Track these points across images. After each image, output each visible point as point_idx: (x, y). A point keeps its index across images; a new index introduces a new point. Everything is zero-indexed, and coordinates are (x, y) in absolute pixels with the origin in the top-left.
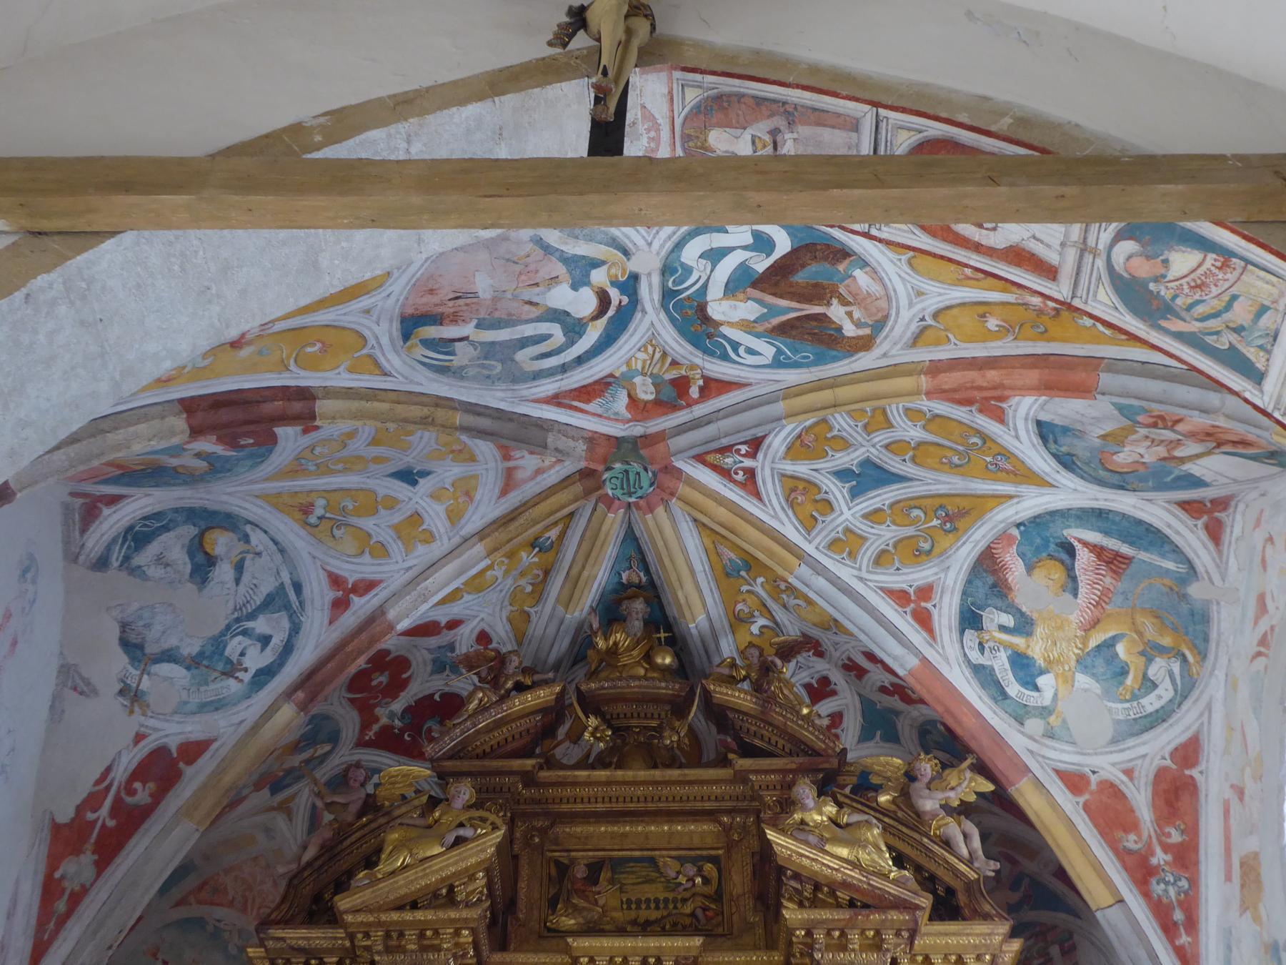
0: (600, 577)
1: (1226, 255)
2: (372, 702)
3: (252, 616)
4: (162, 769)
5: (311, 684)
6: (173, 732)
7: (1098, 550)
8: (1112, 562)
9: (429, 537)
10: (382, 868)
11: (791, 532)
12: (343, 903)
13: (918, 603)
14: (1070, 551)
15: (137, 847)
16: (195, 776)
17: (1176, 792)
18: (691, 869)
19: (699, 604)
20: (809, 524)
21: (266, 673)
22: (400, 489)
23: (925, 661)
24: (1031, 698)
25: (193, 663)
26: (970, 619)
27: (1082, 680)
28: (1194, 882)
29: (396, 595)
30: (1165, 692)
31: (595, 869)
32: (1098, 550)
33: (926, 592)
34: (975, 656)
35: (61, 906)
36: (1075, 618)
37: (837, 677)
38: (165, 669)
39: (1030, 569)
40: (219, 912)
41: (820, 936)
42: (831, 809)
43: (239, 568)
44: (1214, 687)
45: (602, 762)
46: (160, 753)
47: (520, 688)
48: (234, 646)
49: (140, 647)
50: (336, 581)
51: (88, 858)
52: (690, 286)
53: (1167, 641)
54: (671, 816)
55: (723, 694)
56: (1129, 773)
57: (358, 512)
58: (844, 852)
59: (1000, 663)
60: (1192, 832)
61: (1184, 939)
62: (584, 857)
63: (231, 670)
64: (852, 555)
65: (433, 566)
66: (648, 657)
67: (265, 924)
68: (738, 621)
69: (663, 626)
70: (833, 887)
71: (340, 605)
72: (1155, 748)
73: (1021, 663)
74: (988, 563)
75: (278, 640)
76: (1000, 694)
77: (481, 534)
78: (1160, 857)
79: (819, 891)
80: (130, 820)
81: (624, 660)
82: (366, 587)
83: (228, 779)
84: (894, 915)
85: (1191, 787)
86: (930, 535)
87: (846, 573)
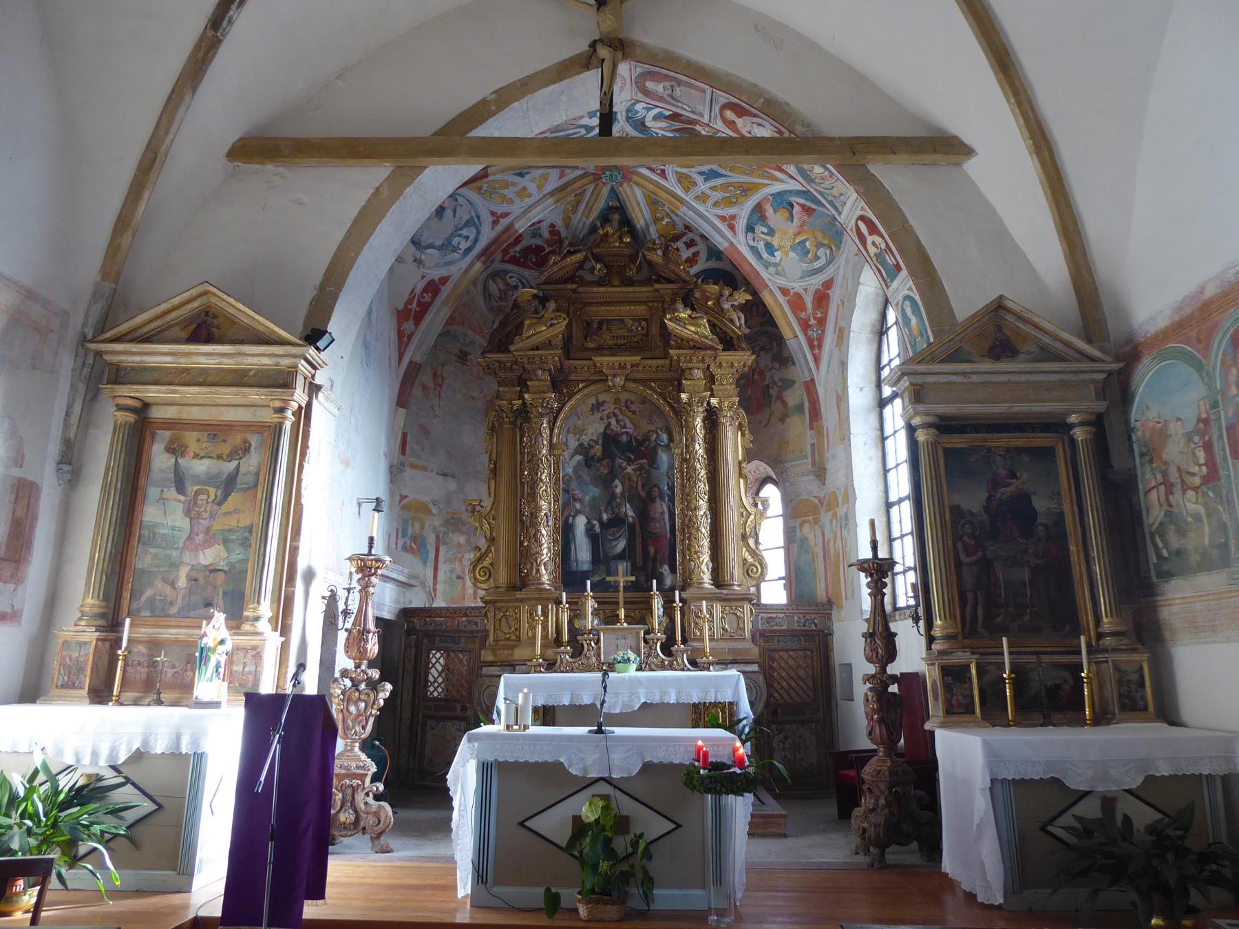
0: (601, 204)
1: (832, 174)
2: (561, 440)
3: (461, 229)
4: (433, 288)
5: (486, 253)
6: (436, 274)
7: (803, 206)
8: (808, 211)
9: (530, 195)
10: (525, 335)
11: (679, 192)
12: (512, 348)
13: (730, 222)
14: (792, 206)
15: (429, 317)
16: (446, 289)
17: (822, 298)
18: (637, 324)
19: (641, 215)
20: (687, 190)
21: (469, 250)
22: (518, 179)
23: (732, 244)
24: (772, 260)
25: (440, 248)
26: (750, 229)
27: (792, 254)
28: (823, 332)
29: (518, 218)
30: (823, 261)
31: (601, 323)
32: (803, 206)
33: (733, 217)
34: (751, 242)
35: (405, 340)
36: (791, 231)
37: (698, 239)
38: (429, 251)
39: (775, 211)
40: (454, 327)
41: (682, 359)
42: (689, 312)
43: (455, 211)
44: (841, 261)
45: (599, 283)
46: (432, 282)
47: (570, 253)
48: (455, 241)
49: (419, 243)
50: (493, 213)
51: (411, 323)
52: (639, 116)
53: (826, 242)
54: (629, 303)
55: (650, 256)
56: (805, 290)
57: (501, 188)
58: (693, 329)
59: (761, 246)
60: (825, 313)
61: (816, 351)
62: (596, 319)
63: (455, 250)
64: (704, 202)
65: (532, 206)
66: (620, 238)
67: (484, 353)
68: (657, 220)
69: (627, 222)
70: (688, 341)
71: (495, 223)
72: (817, 281)
73: (769, 246)
74: (759, 209)
75: (472, 237)
76: (759, 257)
77: (552, 194)
78: (812, 322)
79: (683, 343)
80: (424, 308)
81: (611, 239)
82: (505, 215)
83: (459, 291)
84: (709, 352)
85: (828, 296)
86: (736, 197)
87: (701, 208)
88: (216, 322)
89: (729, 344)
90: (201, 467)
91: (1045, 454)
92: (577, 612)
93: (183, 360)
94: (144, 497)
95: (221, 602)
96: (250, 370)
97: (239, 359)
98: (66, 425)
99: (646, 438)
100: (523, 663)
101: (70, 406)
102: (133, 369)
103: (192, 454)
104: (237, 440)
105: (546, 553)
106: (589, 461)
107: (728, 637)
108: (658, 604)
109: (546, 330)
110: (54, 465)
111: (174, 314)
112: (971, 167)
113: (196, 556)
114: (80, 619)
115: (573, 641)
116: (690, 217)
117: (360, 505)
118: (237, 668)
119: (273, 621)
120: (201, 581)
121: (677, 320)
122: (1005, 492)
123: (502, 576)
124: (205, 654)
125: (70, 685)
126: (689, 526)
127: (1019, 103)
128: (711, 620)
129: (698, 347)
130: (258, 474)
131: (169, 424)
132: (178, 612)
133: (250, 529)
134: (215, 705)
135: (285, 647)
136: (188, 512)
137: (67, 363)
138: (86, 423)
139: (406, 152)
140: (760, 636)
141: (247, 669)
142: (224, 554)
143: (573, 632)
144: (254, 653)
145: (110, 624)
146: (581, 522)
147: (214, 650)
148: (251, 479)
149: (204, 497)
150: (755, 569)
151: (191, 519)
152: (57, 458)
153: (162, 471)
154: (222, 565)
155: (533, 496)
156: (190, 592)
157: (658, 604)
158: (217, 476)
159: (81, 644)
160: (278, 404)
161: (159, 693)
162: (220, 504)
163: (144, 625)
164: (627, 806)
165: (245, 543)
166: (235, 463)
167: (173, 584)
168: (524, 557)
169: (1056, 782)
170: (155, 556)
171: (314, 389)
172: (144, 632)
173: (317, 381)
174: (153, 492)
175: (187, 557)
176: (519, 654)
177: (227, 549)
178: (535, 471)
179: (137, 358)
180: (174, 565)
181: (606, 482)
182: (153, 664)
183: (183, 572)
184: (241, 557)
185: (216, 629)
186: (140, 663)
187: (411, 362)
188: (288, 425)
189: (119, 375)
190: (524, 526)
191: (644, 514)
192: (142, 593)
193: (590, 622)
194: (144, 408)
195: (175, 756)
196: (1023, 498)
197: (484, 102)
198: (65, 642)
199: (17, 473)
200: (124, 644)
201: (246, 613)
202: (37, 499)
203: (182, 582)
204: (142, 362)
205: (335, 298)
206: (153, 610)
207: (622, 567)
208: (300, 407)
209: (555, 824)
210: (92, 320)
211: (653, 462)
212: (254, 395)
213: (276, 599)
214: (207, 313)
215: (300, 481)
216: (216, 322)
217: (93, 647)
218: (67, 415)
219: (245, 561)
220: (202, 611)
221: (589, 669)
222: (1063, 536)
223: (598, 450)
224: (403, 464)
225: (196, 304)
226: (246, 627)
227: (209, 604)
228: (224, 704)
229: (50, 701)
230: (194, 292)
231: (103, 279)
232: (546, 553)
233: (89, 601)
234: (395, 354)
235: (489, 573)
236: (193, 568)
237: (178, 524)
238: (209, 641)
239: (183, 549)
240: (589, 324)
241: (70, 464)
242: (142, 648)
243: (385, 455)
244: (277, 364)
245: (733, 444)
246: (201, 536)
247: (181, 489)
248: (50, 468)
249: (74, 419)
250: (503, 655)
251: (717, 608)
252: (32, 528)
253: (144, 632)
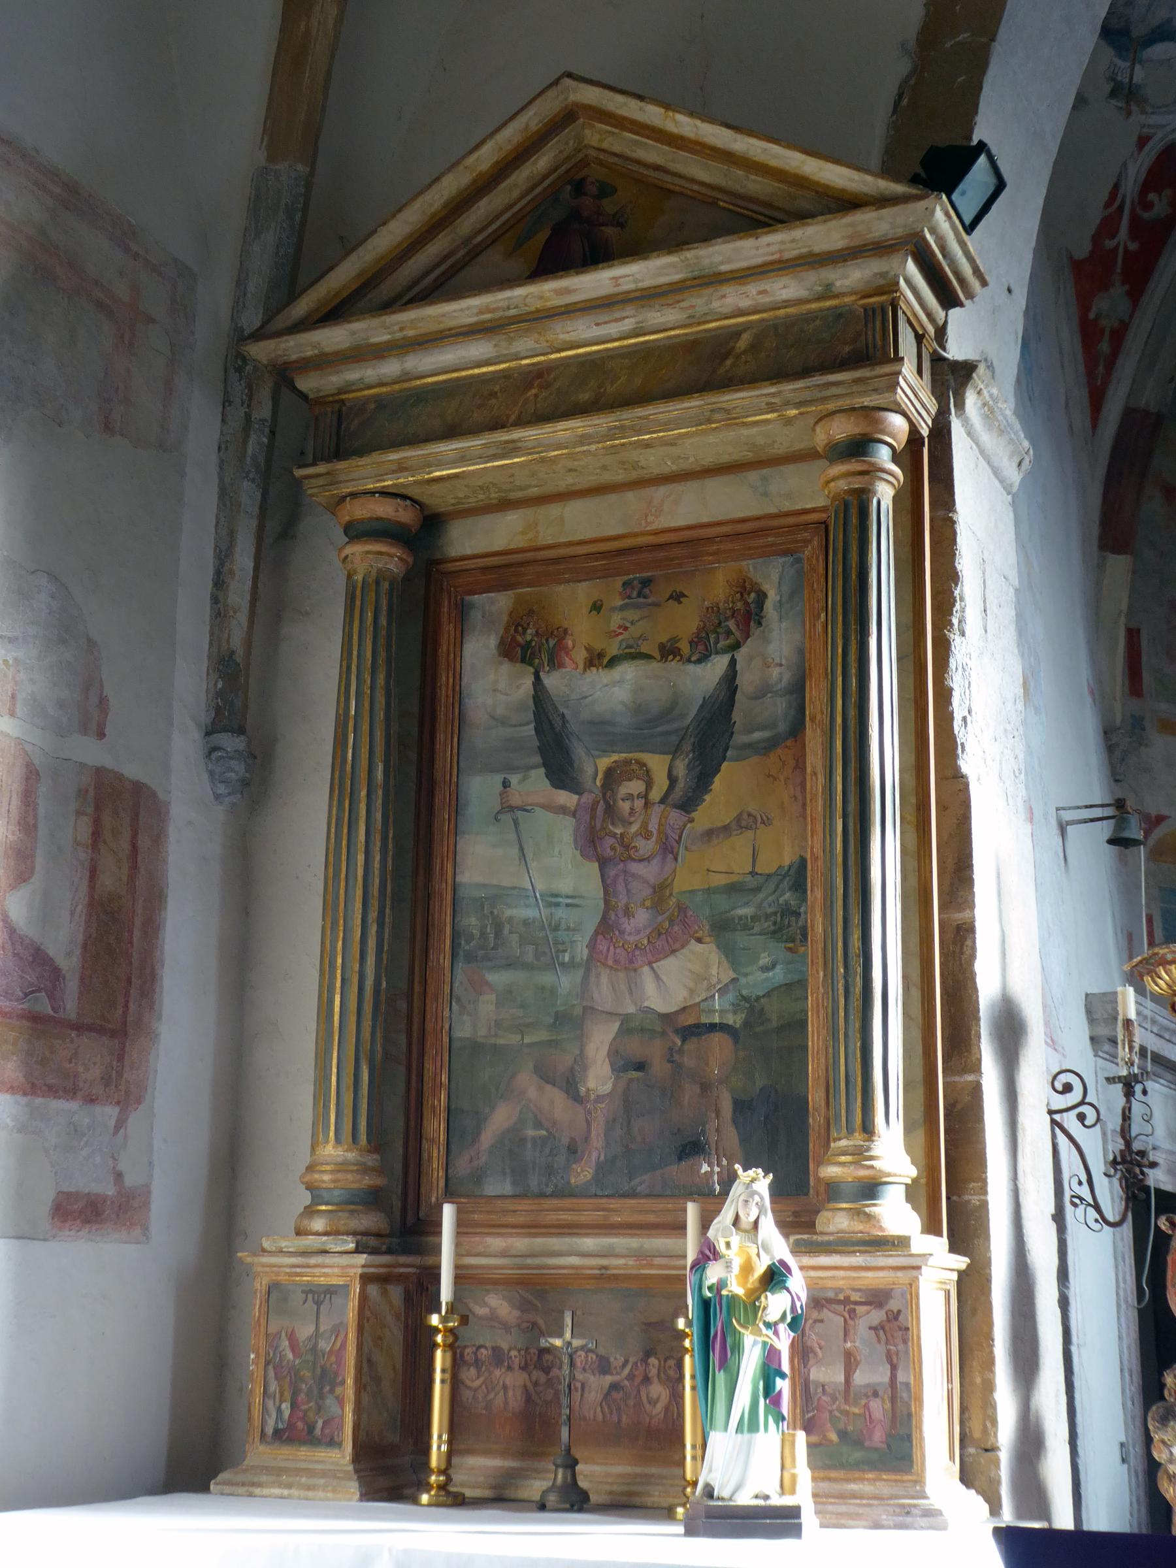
35: (1105, 347)
38: (1159, 50)
49: (1125, 32)
51: (1118, 291)
88: (609, 206)
90: (614, 691)
93: (524, 344)
94: (457, 808)
95: (731, 1137)
96: (737, 333)
97: (699, 302)
98: (220, 613)
101: (224, 555)
102: (381, 403)
103: (581, 655)
104: (716, 586)
110: (196, 735)
111: (484, 208)
113: (633, 988)
114: (310, 1212)
117: (1062, 828)
118: (827, 1374)
119: (923, 1194)
120: (659, 1068)
124: (718, 1324)
125: (297, 1433)
130: (798, 688)
131: (503, 571)
132: (598, 1179)
133: (797, 877)
134: (777, 1521)
135: (971, 1289)
136: (590, 842)
137: (201, 425)
138: (273, 606)
141: (860, 1378)
142: (719, 970)
144: (877, 1316)
145: (398, 1225)
147: (751, 1309)
148: (778, 708)
149: (635, 787)
151: (603, 863)
152: (206, 718)
153: (503, 722)
154: (720, 1009)
156: (628, 1106)
158: (667, 713)
159: (322, 1295)
160: (841, 429)
161: (571, 1464)
162: (688, 805)
163: (495, 1227)
165: (787, 928)
166: (719, 664)
167: (571, 1085)
170: (507, 996)
171: (950, 378)
172: (501, 1250)
173: (955, 351)
174: (479, 790)
175: (605, 990)
177: (729, 952)
179: (390, 368)
180: (570, 1022)
182: (540, 1360)
183: (600, 1041)
184: (778, 975)
185: (744, 1234)
186: (498, 1356)
187: (1129, 413)
188: (885, 494)
189: (345, 429)
192: (480, 1120)
194: (421, 530)
198: (273, 1288)
199: (92, 753)
200: (446, 1294)
201: (831, 1171)
202: (158, 839)
203: (599, 1078)
204: (406, 377)
205: (977, 63)
206: (519, 1173)
208: (914, 438)
210: (256, 284)
212: (762, 415)
213: (921, 1119)
214: (579, 187)
215: (944, 695)
216: (609, 206)
217: (353, 1304)
218: (220, 583)
219: (796, 987)
220: (676, 1171)
224: (1137, 725)
225: (542, 162)
226: (837, 1221)
227: (692, 1148)
228: (809, 1518)
229: (248, 1488)
230: (532, 119)
231: (272, 158)
233: (330, 1151)
234: (1081, 394)
236: (628, 1028)
237: (565, 886)
238: (730, 1274)
239: (588, 965)
241: (241, 731)
242: (497, 1304)
243: (1092, 693)
244: (828, 292)
246: (642, 917)
247: (561, 772)
248: (185, 745)
249: (239, 594)
252: (152, 928)
253: (501, 1250)
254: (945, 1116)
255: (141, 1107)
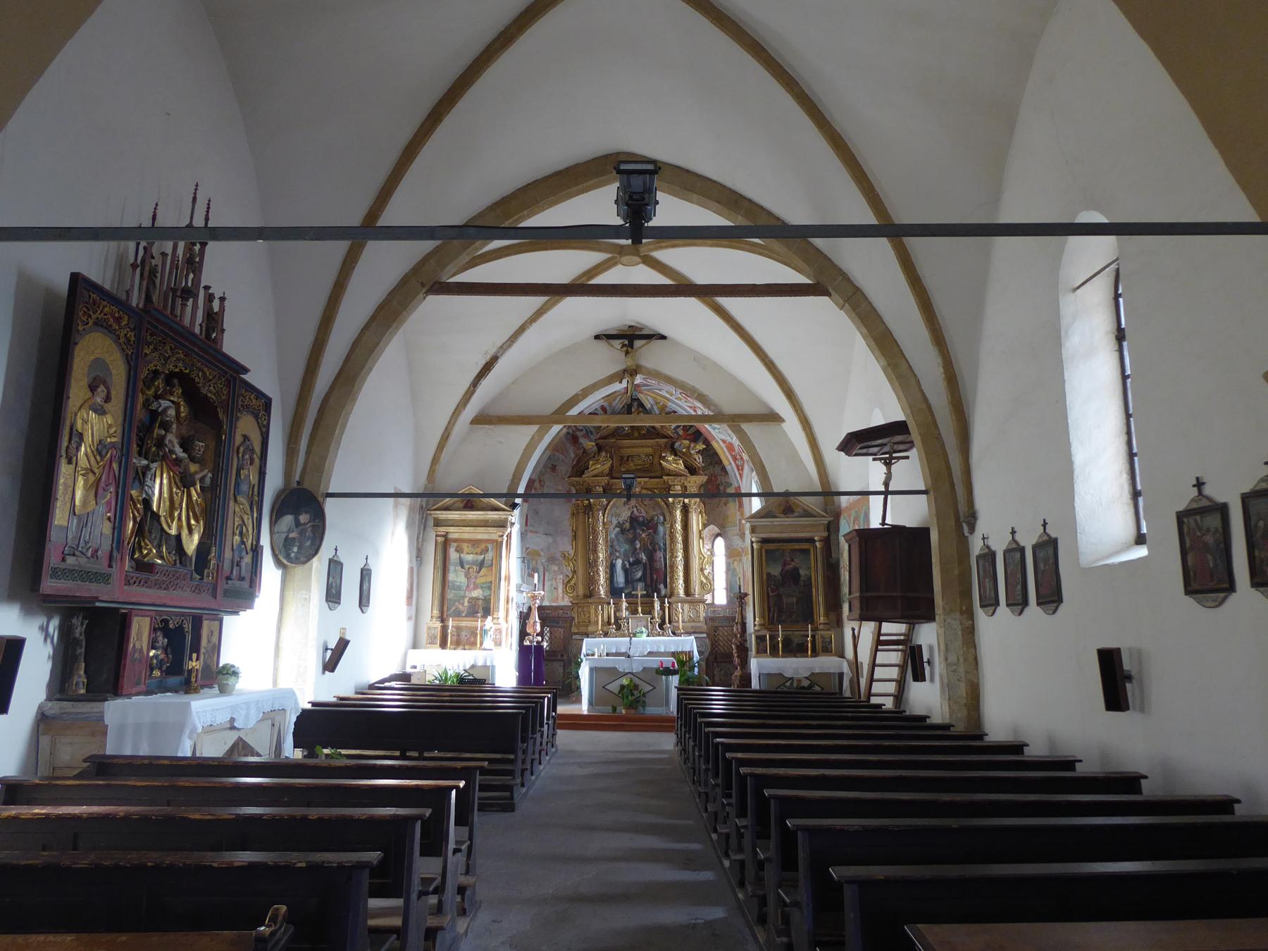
89: (692, 470)
90: (470, 558)
91: (806, 552)
92: (618, 609)
99: (652, 519)
100: (593, 633)
104: (483, 546)
105: (602, 580)
106: (623, 531)
107: (691, 620)
108: (657, 605)
109: (600, 466)
112: (784, 425)
115: (616, 622)
116: (674, 407)
121: (667, 461)
122: (789, 567)
123: (581, 591)
126: (673, 566)
127: (796, 411)
128: (683, 613)
129: (677, 475)
131: (456, 540)
139: (543, 421)
140: (709, 619)
143: (617, 619)
146: (619, 563)
150: (708, 586)
155: (595, 551)
156: (469, 608)
157: (657, 605)
164: (637, 681)
168: (591, 581)
169: (781, 675)
174: (452, 568)
176: (590, 629)
178: (595, 538)
180: (464, 597)
181: (632, 542)
189: (438, 523)
190: (591, 565)
191: (651, 558)
193: (625, 613)
194: (445, 536)
195: (485, 667)
196: (796, 569)
197: (576, 395)
207: (640, 585)
209: (614, 687)
211: (655, 531)
221: (624, 636)
222: (810, 584)
223: (627, 525)
232: (602, 580)
235: (574, 588)
240: (622, 458)
245: (696, 521)
250: (582, 629)
251: (686, 606)
253: (456, 623)
254: (798, 799)
255: (1062, 607)
